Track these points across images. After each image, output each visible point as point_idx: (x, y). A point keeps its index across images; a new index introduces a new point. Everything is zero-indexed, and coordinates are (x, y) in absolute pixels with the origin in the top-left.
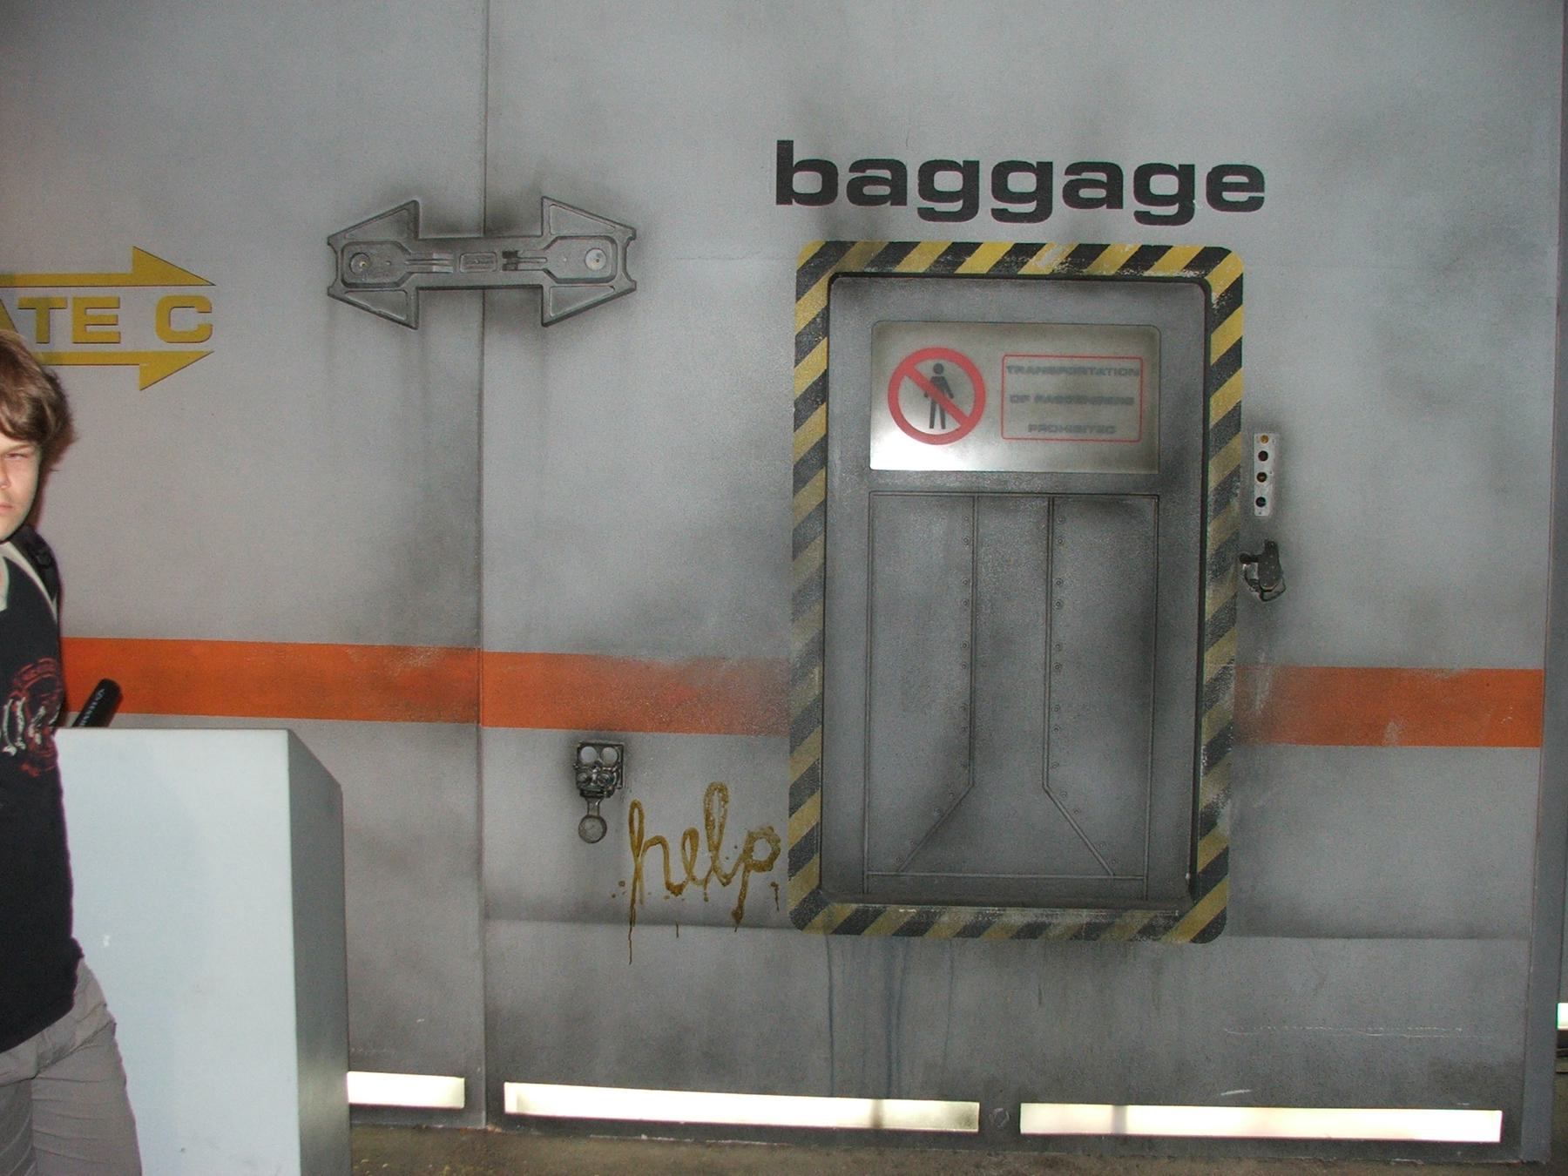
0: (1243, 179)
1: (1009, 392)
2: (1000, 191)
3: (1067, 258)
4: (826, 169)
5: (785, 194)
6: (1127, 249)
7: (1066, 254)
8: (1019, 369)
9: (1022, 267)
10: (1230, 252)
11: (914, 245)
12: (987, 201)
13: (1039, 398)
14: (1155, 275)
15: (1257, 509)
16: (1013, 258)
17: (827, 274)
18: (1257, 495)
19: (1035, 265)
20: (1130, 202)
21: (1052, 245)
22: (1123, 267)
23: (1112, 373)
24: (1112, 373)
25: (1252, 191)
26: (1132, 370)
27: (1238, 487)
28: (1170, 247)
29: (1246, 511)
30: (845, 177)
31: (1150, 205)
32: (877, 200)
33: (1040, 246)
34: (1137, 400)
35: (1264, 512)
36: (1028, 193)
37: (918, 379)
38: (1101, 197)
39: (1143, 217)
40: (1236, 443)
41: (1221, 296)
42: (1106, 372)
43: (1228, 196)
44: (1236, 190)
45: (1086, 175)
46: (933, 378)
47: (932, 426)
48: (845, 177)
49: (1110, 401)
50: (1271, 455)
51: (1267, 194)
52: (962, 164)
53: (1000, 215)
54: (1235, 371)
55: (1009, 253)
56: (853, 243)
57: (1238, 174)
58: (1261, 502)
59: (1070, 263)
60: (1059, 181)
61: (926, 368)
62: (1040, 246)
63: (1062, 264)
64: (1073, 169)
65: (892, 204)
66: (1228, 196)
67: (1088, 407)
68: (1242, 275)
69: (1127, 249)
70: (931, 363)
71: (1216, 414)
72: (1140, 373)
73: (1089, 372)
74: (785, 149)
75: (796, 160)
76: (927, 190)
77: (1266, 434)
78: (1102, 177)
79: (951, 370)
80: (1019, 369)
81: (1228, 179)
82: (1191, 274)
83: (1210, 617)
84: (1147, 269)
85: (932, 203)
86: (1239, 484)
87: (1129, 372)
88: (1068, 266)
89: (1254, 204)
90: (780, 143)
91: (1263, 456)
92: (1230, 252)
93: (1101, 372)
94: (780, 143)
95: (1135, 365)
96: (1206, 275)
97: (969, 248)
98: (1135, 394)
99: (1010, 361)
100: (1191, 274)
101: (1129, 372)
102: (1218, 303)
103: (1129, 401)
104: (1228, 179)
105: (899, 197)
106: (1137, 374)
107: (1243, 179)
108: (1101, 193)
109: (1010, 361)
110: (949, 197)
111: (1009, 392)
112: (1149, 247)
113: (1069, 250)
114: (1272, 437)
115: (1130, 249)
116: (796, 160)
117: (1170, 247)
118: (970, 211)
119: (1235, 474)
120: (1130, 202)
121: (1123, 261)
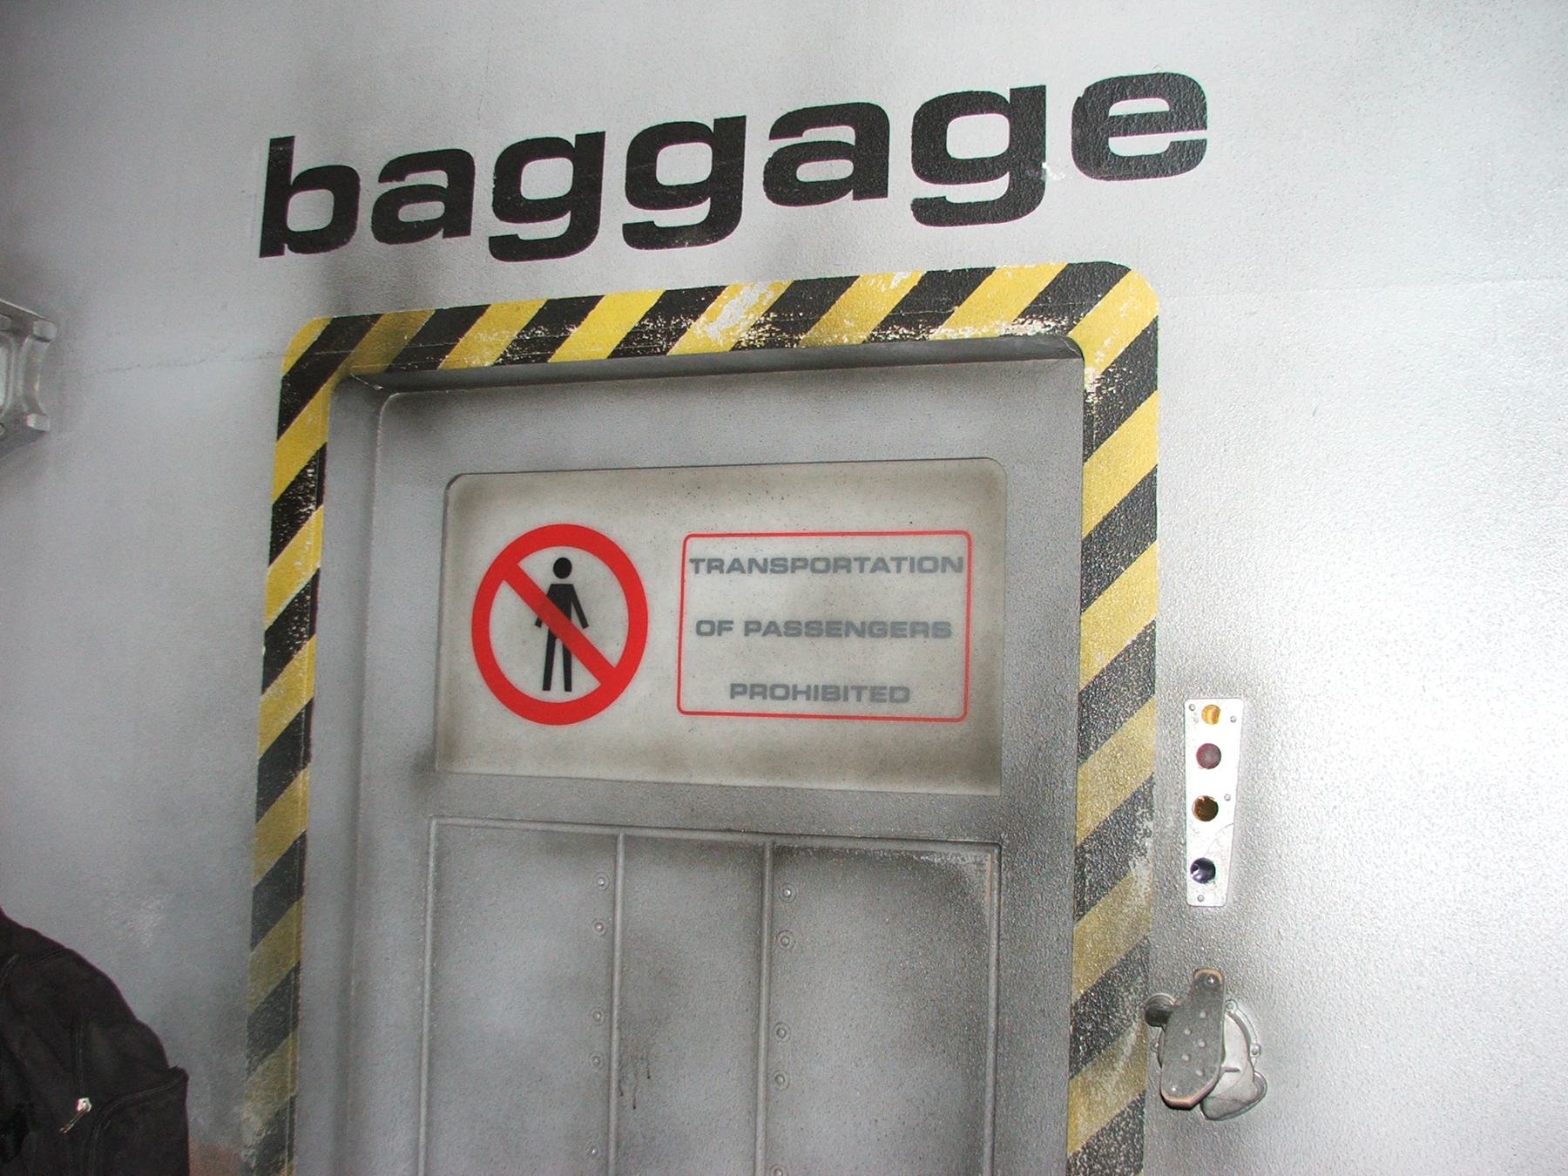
0: (1158, 105)
1: (693, 614)
2: (643, 187)
3: (767, 314)
4: (340, 181)
5: (276, 238)
6: (893, 285)
7: (766, 304)
8: (715, 565)
9: (676, 340)
10: (1126, 270)
11: (479, 311)
12: (616, 209)
13: (751, 627)
14: (955, 337)
15: (1196, 892)
16: (661, 322)
17: (330, 380)
18: (1193, 854)
19: (963, 325)
20: (485, 220)
21: (737, 289)
22: (886, 324)
23: (906, 566)
24: (906, 566)
25: (1179, 129)
26: (946, 560)
27: (1146, 834)
28: (989, 271)
29: (1169, 888)
30: (371, 191)
31: (945, 182)
32: (422, 231)
33: (713, 292)
34: (958, 629)
35: (1203, 896)
36: (993, 159)
37: (525, 587)
38: (843, 176)
39: (931, 212)
40: (1142, 727)
41: (1106, 373)
42: (892, 566)
43: (1121, 146)
44: (1140, 131)
45: (812, 135)
46: (553, 586)
47: (547, 685)
48: (371, 191)
49: (896, 630)
50: (1230, 758)
51: (1216, 133)
52: (573, 142)
53: (640, 236)
54: (1139, 549)
55: (652, 314)
56: (376, 317)
57: (1146, 95)
58: (1206, 869)
59: (774, 323)
60: (758, 151)
61: (539, 566)
62: (713, 292)
63: (756, 326)
64: (788, 125)
65: (855, 198)
66: (1121, 146)
67: (853, 643)
68: (1155, 321)
69: (893, 285)
70: (548, 556)
71: (1097, 656)
72: (962, 565)
73: (855, 566)
74: (281, 150)
75: (297, 169)
76: (510, 203)
77: (1214, 702)
78: (845, 134)
79: (589, 573)
80: (715, 565)
81: (1119, 109)
82: (1035, 327)
83: (1071, 1154)
84: (936, 325)
85: (939, 186)
86: (1150, 825)
87: (943, 564)
88: (770, 331)
89: (1186, 157)
90: (275, 143)
91: (1209, 756)
92: (1126, 270)
93: (881, 565)
94: (275, 143)
95: (952, 547)
96: (1071, 327)
97: (572, 310)
98: (956, 617)
99: (697, 548)
100: (1035, 327)
101: (943, 564)
102: (1099, 390)
103: (941, 630)
104: (1119, 109)
105: (457, 222)
106: (958, 568)
107: (1158, 105)
108: (842, 169)
109: (697, 548)
110: (684, 196)
111: (693, 614)
112: (941, 274)
113: (772, 297)
114: (1231, 707)
115: (902, 282)
116: (297, 169)
117: (989, 271)
118: (722, 223)
119: (1142, 799)
120: (485, 220)
121: (885, 309)
